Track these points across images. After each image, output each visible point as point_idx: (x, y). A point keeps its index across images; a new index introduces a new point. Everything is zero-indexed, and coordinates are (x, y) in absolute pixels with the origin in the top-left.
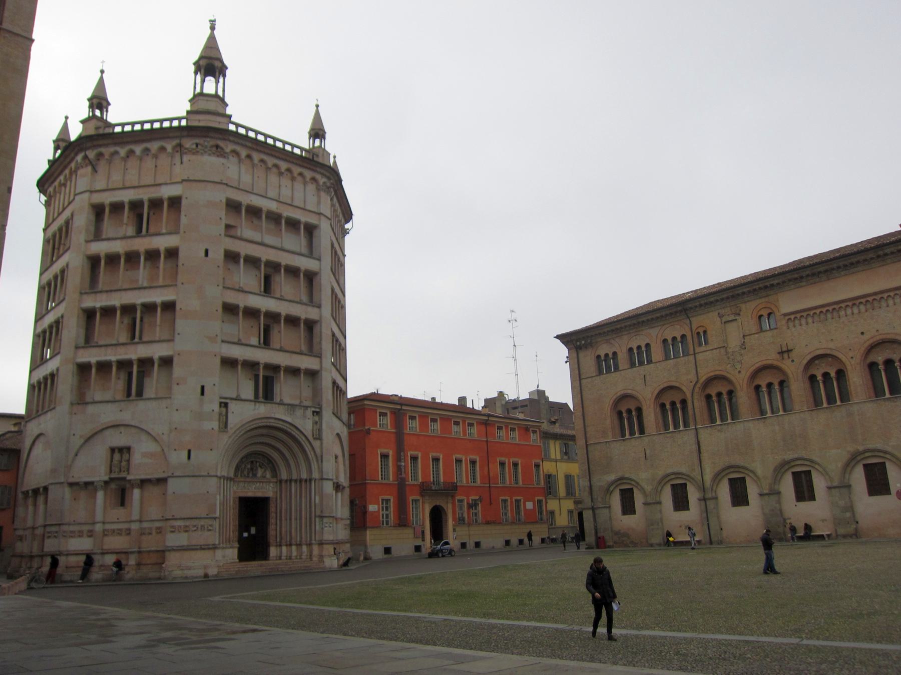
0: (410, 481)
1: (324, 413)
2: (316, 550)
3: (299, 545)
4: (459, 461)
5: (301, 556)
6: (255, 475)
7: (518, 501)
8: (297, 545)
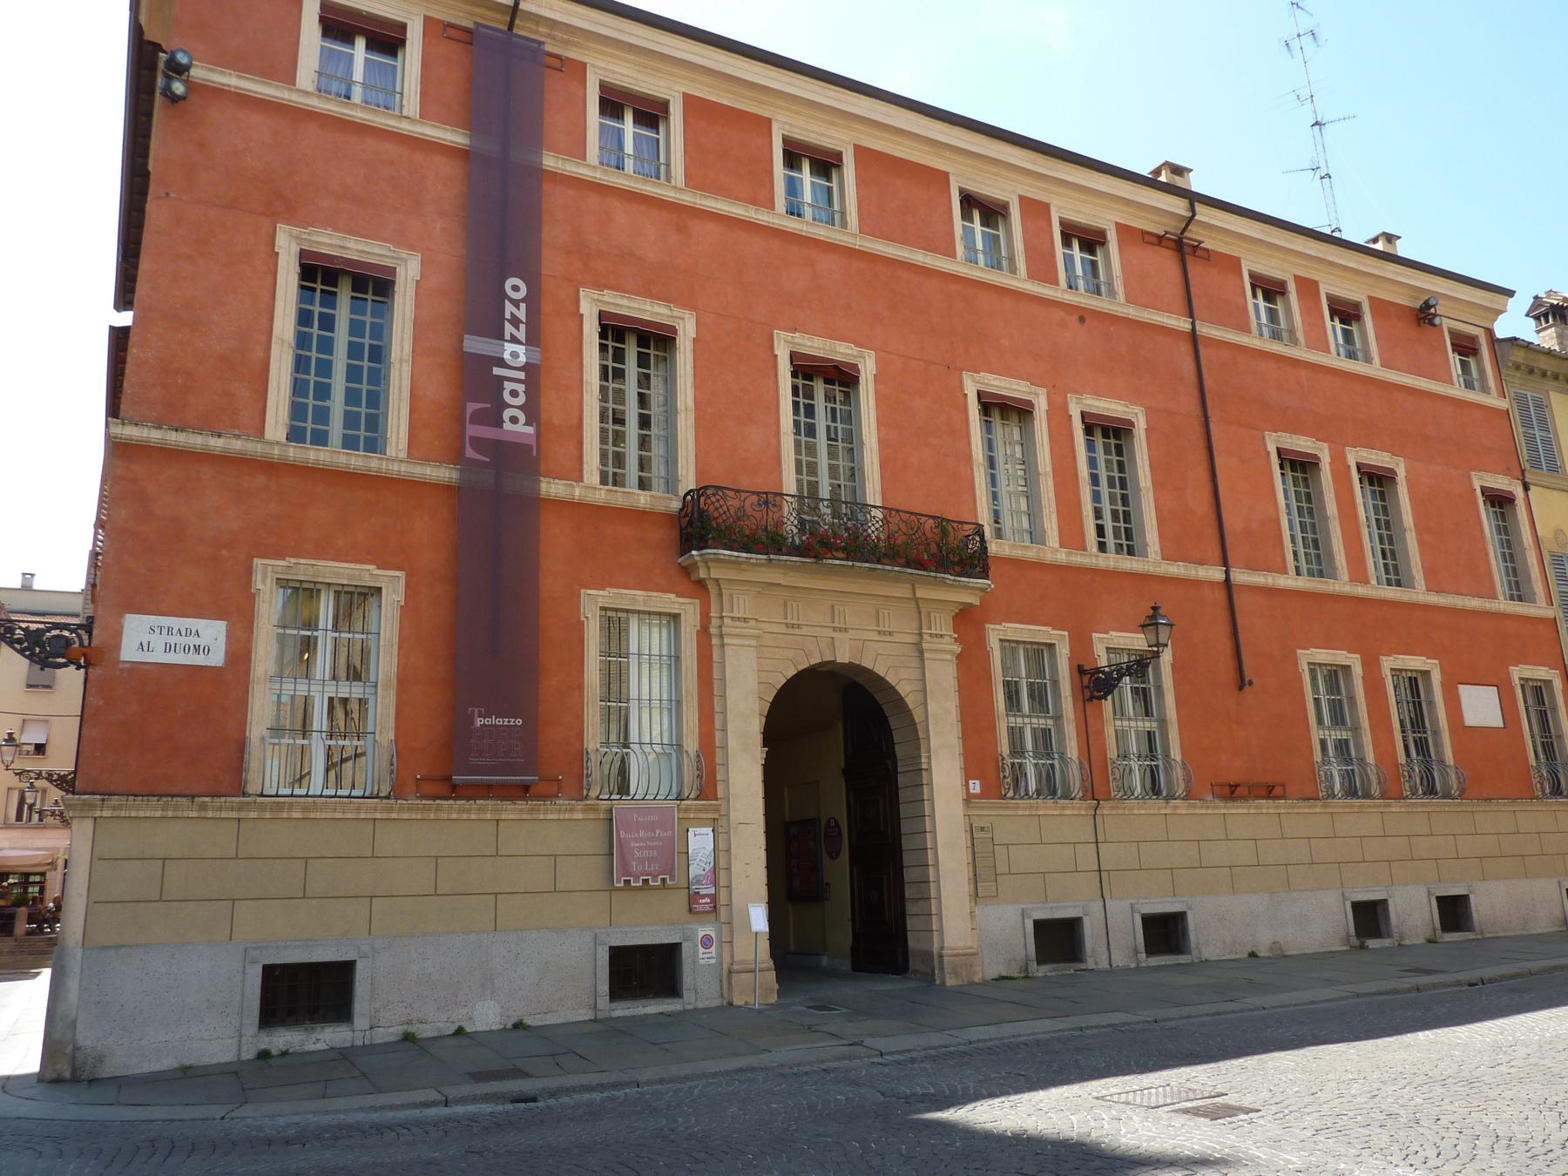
7: (1414, 684)
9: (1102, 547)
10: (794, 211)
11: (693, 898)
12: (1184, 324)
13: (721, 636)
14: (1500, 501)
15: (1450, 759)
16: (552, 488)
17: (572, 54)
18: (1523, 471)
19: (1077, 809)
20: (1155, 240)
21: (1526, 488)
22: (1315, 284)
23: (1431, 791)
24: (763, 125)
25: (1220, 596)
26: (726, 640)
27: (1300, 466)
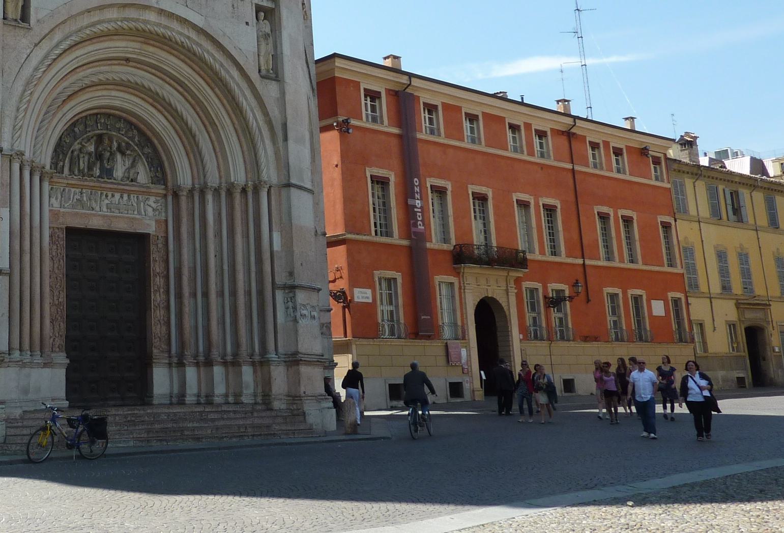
0: (434, 243)
1: (284, 13)
2: (279, 376)
3: (233, 364)
4: (524, 205)
5: (238, 395)
6: (108, 173)
7: (637, 299)
8: (225, 364)
9: (376, 234)
10: (531, 153)
11: (463, 369)
12: (569, 166)
13: (464, 289)
14: (666, 226)
15: (648, 328)
16: (428, 245)
17: (416, 94)
18: (675, 214)
19: (545, 344)
20: (561, 133)
21: (675, 221)
22: (530, 125)
23: (641, 339)
24: (357, 84)
25: (581, 269)
26: (466, 291)
27: (604, 217)
